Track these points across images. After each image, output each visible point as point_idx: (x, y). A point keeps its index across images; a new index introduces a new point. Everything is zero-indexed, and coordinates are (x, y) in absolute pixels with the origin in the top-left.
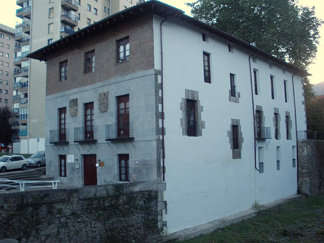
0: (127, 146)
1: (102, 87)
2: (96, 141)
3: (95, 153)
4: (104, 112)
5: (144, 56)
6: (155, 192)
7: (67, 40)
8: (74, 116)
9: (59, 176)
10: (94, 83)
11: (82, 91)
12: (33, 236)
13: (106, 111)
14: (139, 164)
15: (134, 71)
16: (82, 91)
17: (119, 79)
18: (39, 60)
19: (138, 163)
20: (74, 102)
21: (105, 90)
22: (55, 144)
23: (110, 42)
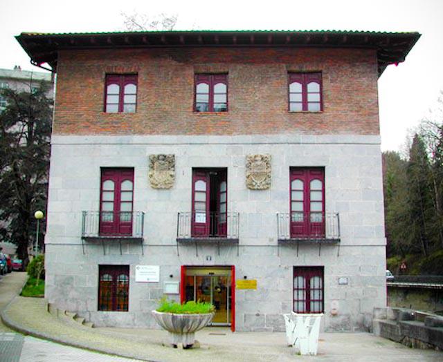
0: (199, 254)
1: (253, 144)
2: (237, 241)
3: (322, 265)
4: (264, 189)
5: (358, 111)
6: (101, 274)
7: (38, 214)
8: (165, 188)
9: (194, 336)
10: (230, 134)
11: (191, 144)
12: (14, 255)
13: (268, 188)
14: (347, 284)
15: (335, 131)
16: (191, 144)
17: (301, 137)
18: (30, 59)
19: (345, 282)
20: (167, 162)
21: (262, 151)
22: (89, 240)
23: (274, 69)
